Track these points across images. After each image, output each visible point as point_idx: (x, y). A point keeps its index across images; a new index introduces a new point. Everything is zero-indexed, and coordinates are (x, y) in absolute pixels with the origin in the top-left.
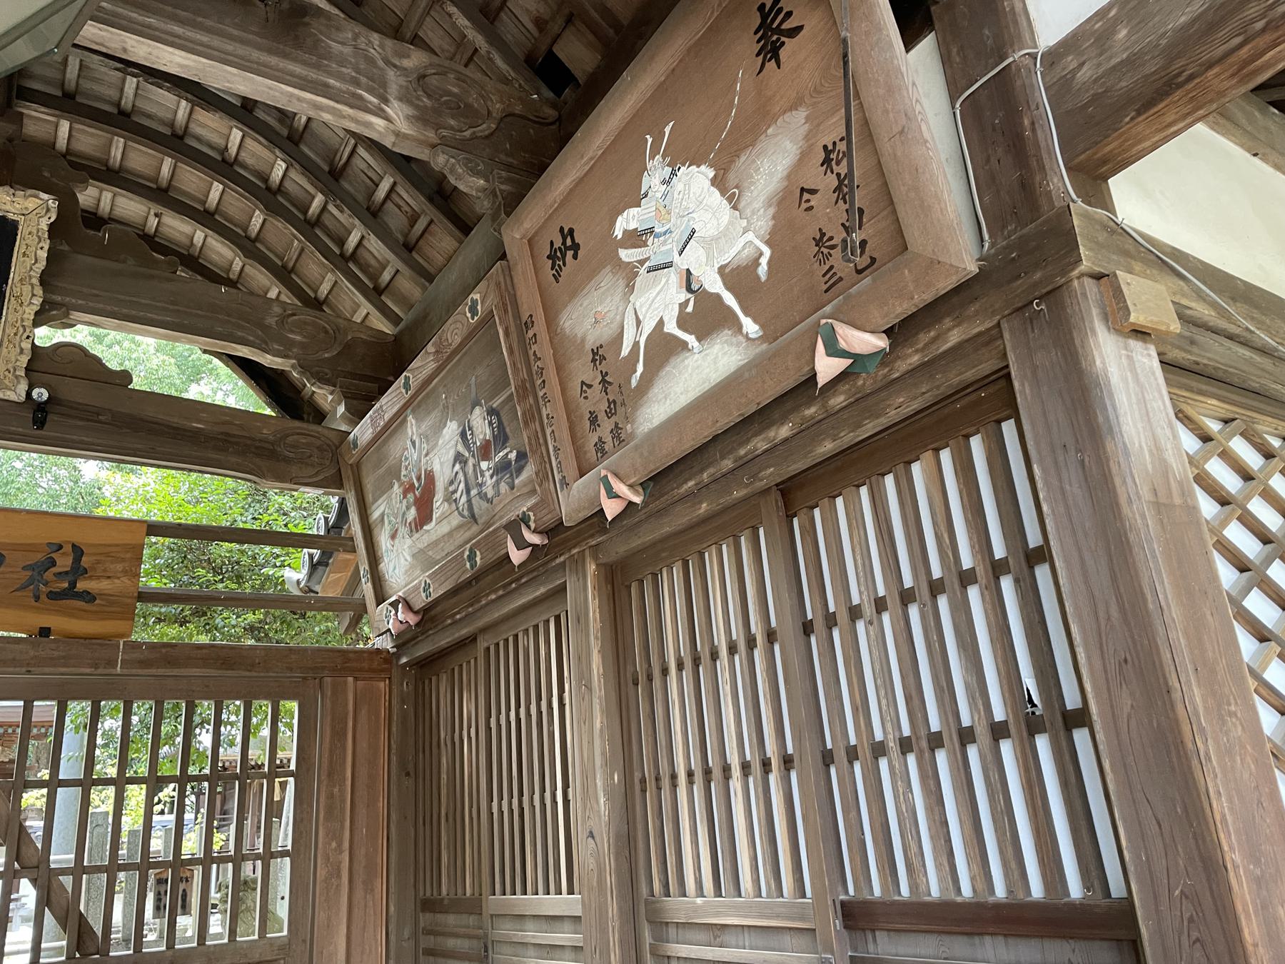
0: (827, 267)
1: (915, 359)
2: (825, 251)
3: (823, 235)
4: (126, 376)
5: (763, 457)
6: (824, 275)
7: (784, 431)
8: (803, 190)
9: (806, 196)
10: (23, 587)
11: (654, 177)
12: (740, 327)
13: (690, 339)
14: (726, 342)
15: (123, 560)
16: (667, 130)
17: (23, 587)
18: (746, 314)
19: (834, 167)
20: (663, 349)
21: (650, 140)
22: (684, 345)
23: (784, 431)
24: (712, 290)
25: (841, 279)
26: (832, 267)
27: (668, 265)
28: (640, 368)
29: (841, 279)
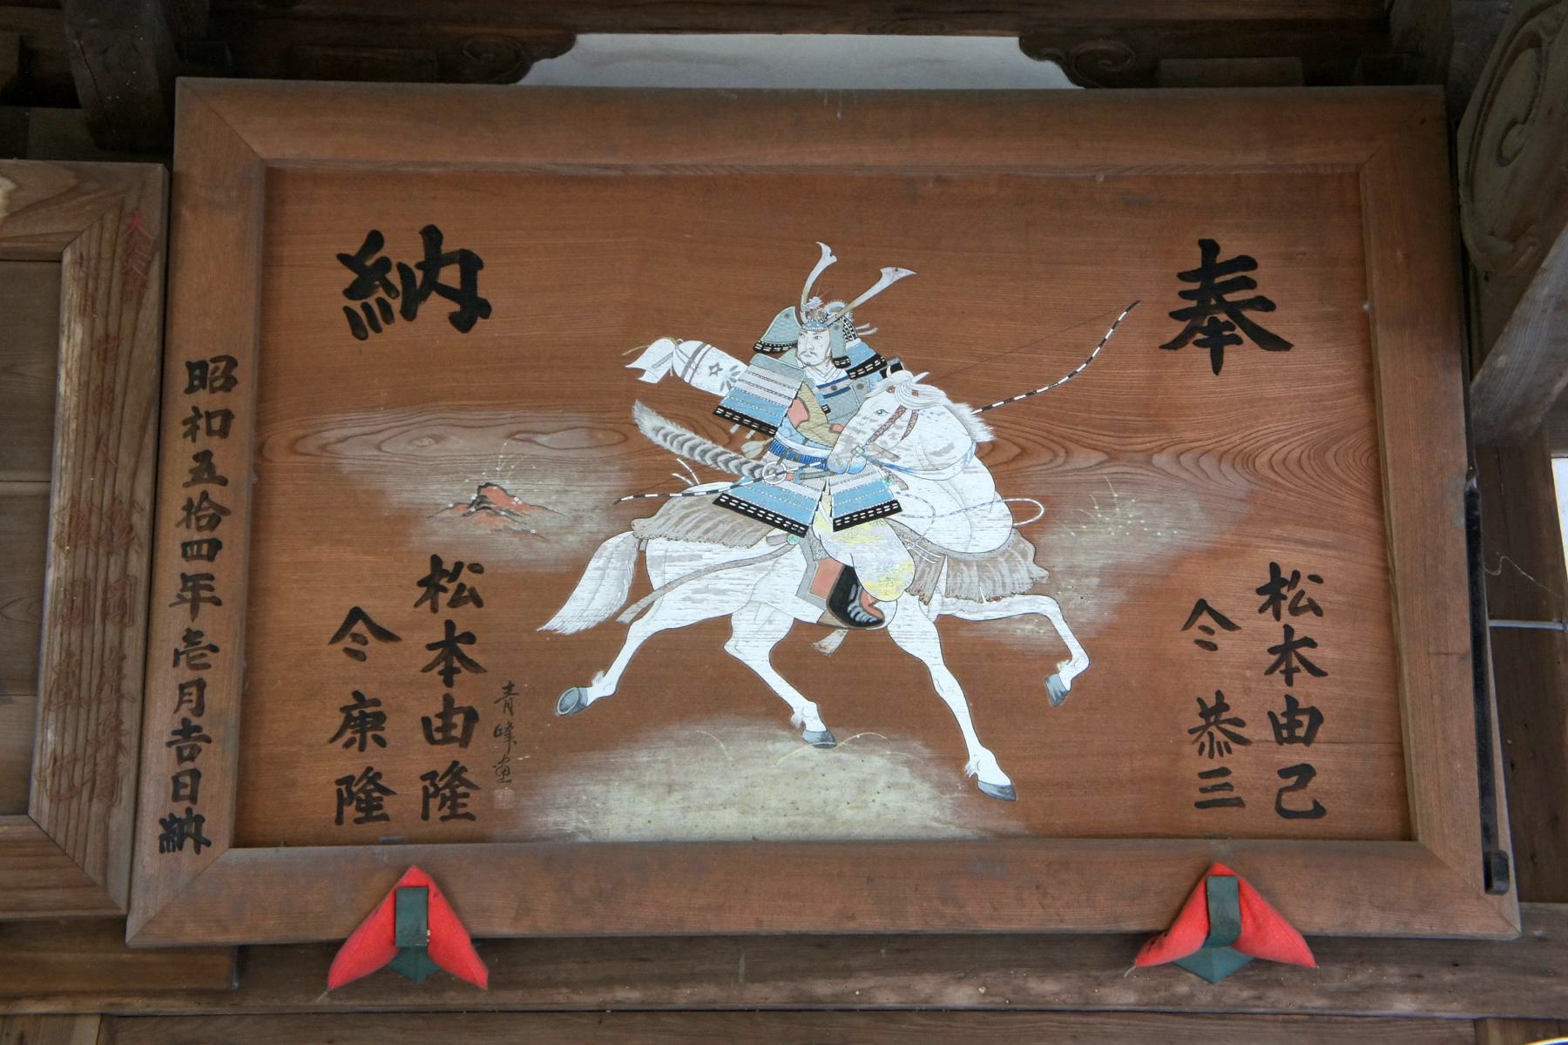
0: (1214, 765)
1: (1318, 1003)
2: (1220, 737)
3: (1221, 706)
4: (984, 452)
5: (861, 1021)
6: (1203, 775)
7: (962, 995)
8: (1202, 606)
9: (1205, 619)
10: (1270, 671)
11: (816, 341)
12: (962, 756)
13: (806, 711)
14: (909, 763)
15: (442, 520)
16: (889, 277)
17: (1270, 671)
18: (985, 741)
19: (1285, 611)
20: (694, 681)
21: (827, 258)
22: (780, 711)
23: (962, 995)
24: (910, 648)
25: (1239, 802)
26: (1224, 772)
27: (798, 530)
28: (603, 686)
29: (1239, 802)
